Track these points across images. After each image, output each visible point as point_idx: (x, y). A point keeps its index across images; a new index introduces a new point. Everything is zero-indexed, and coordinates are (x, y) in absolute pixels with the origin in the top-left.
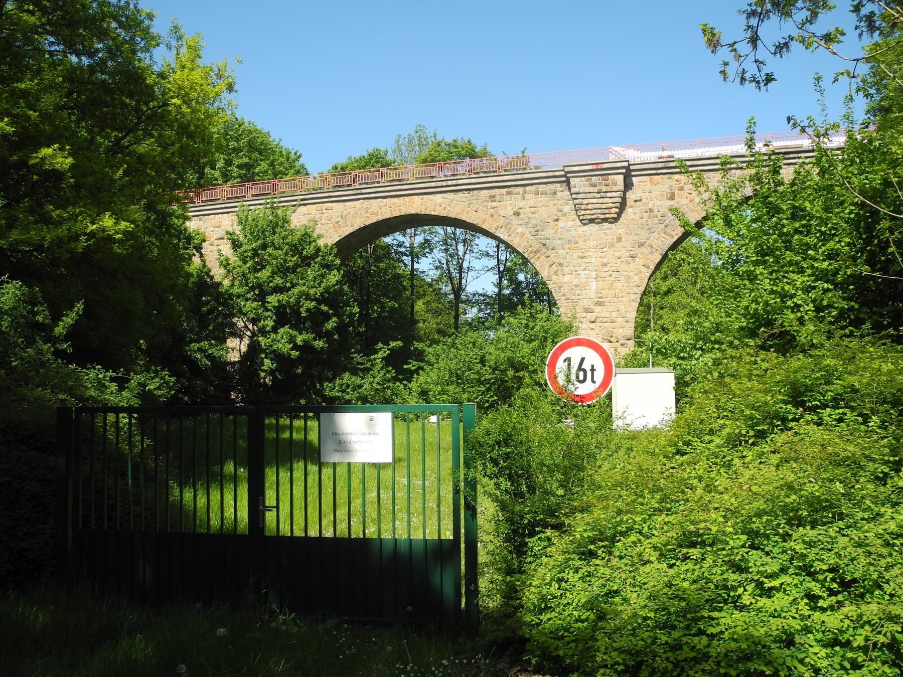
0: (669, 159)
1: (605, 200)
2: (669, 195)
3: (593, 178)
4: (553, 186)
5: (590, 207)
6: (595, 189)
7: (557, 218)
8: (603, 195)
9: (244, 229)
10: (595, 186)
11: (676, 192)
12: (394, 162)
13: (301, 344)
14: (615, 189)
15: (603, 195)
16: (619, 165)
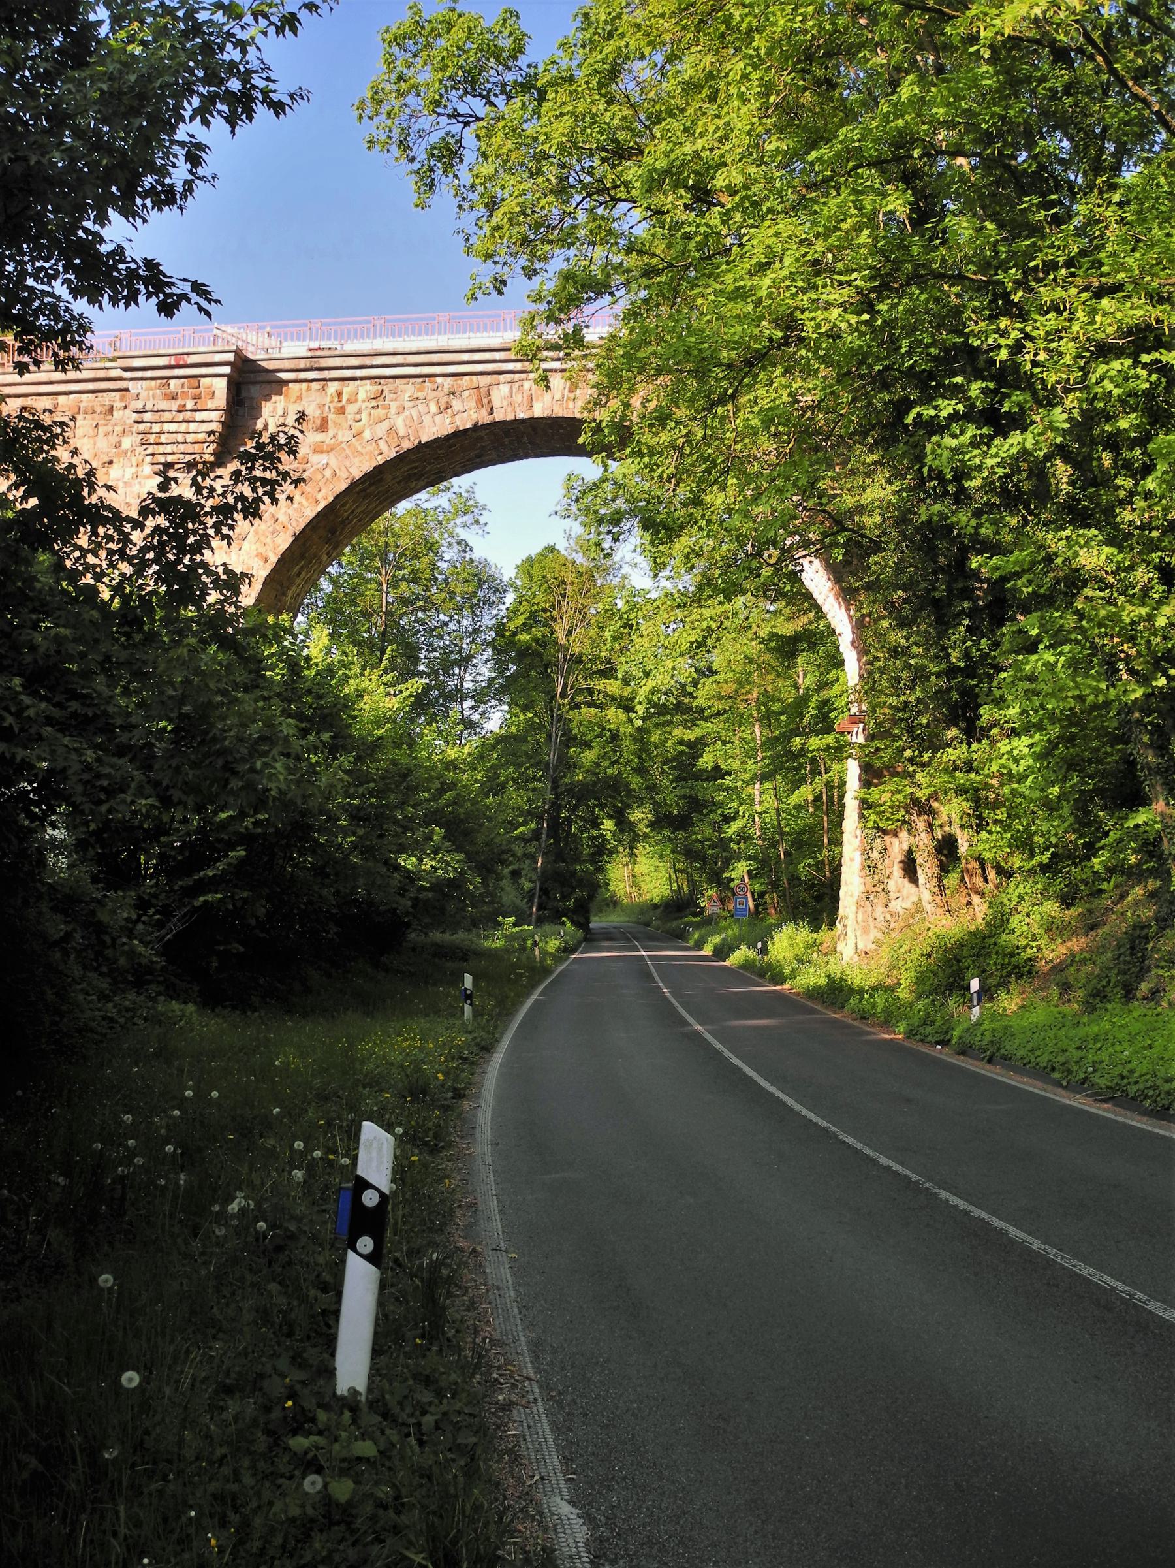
0: (318, 353)
1: (193, 427)
2: (318, 422)
3: (172, 382)
4: (106, 398)
5: (163, 439)
6: (174, 405)
7: (107, 459)
8: (188, 415)
9: (974, 216)
10: (174, 397)
11: (331, 417)
12: (450, 26)
13: (345, 1393)
14: (210, 405)
15: (188, 415)
16: (217, 358)
